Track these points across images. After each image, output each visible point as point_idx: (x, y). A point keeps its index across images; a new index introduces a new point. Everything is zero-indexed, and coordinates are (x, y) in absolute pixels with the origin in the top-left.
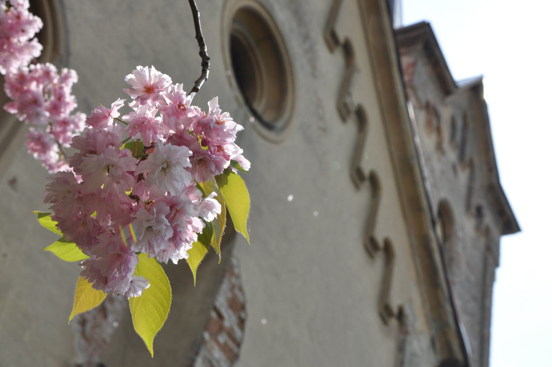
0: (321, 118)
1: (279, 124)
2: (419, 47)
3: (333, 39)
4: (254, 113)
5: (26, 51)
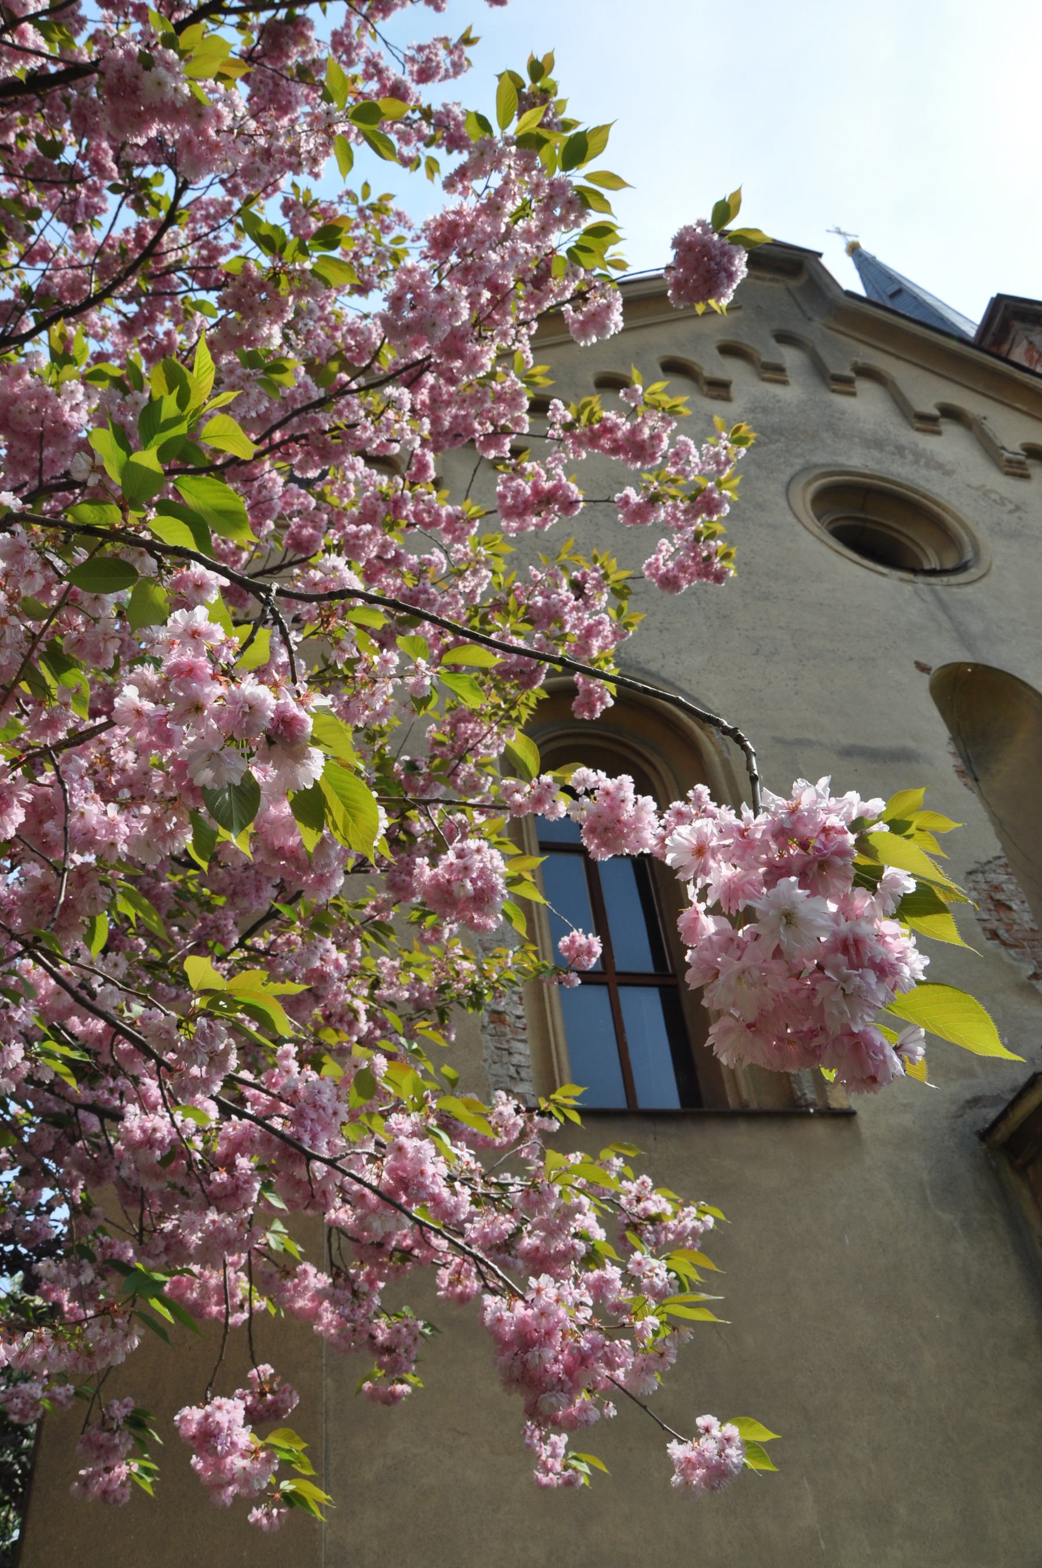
0: (1002, 501)
1: (969, 555)
2: (1017, 325)
3: (926, 423)
4: (932, 573)
5: (644, 815)
